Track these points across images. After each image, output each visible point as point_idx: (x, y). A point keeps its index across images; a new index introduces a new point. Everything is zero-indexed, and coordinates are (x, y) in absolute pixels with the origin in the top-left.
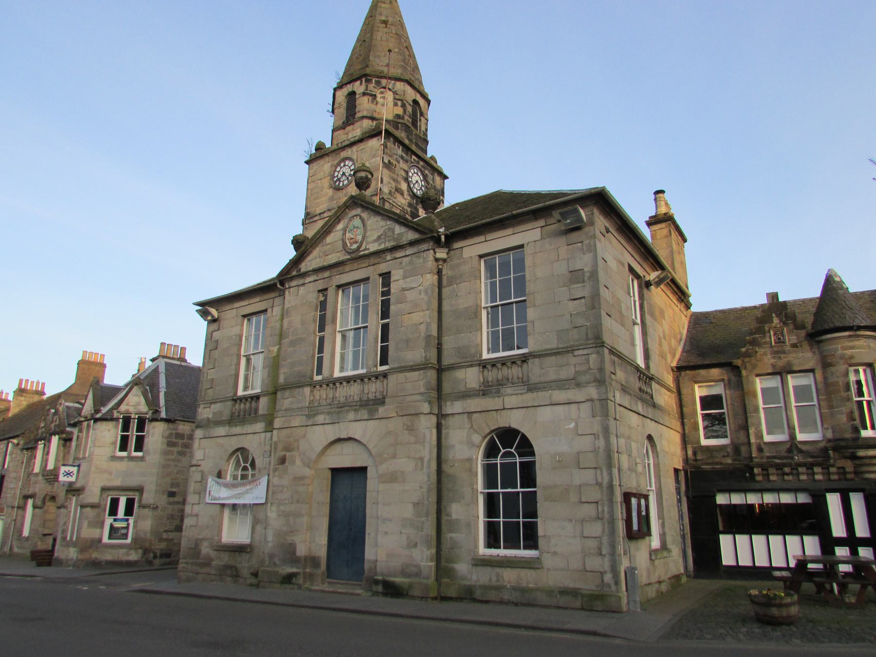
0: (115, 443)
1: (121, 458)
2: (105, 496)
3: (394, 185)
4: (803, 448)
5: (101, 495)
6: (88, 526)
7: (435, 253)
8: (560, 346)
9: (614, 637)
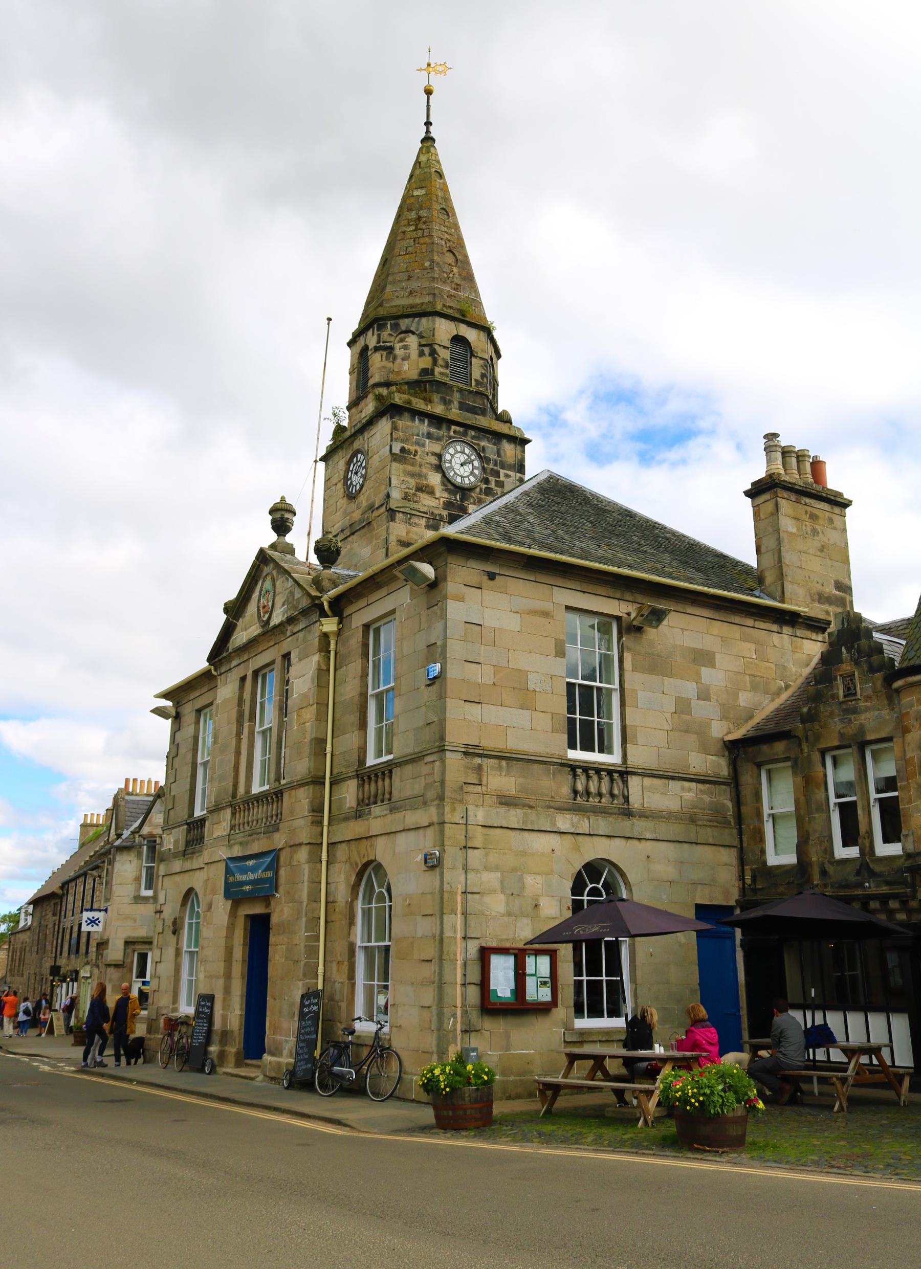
0: (138, 879)
1: (146, 899)
2: (129, 951)
3: (412, 482)
4: (877, 868)
5: (125, 950)
8: (416, 750)
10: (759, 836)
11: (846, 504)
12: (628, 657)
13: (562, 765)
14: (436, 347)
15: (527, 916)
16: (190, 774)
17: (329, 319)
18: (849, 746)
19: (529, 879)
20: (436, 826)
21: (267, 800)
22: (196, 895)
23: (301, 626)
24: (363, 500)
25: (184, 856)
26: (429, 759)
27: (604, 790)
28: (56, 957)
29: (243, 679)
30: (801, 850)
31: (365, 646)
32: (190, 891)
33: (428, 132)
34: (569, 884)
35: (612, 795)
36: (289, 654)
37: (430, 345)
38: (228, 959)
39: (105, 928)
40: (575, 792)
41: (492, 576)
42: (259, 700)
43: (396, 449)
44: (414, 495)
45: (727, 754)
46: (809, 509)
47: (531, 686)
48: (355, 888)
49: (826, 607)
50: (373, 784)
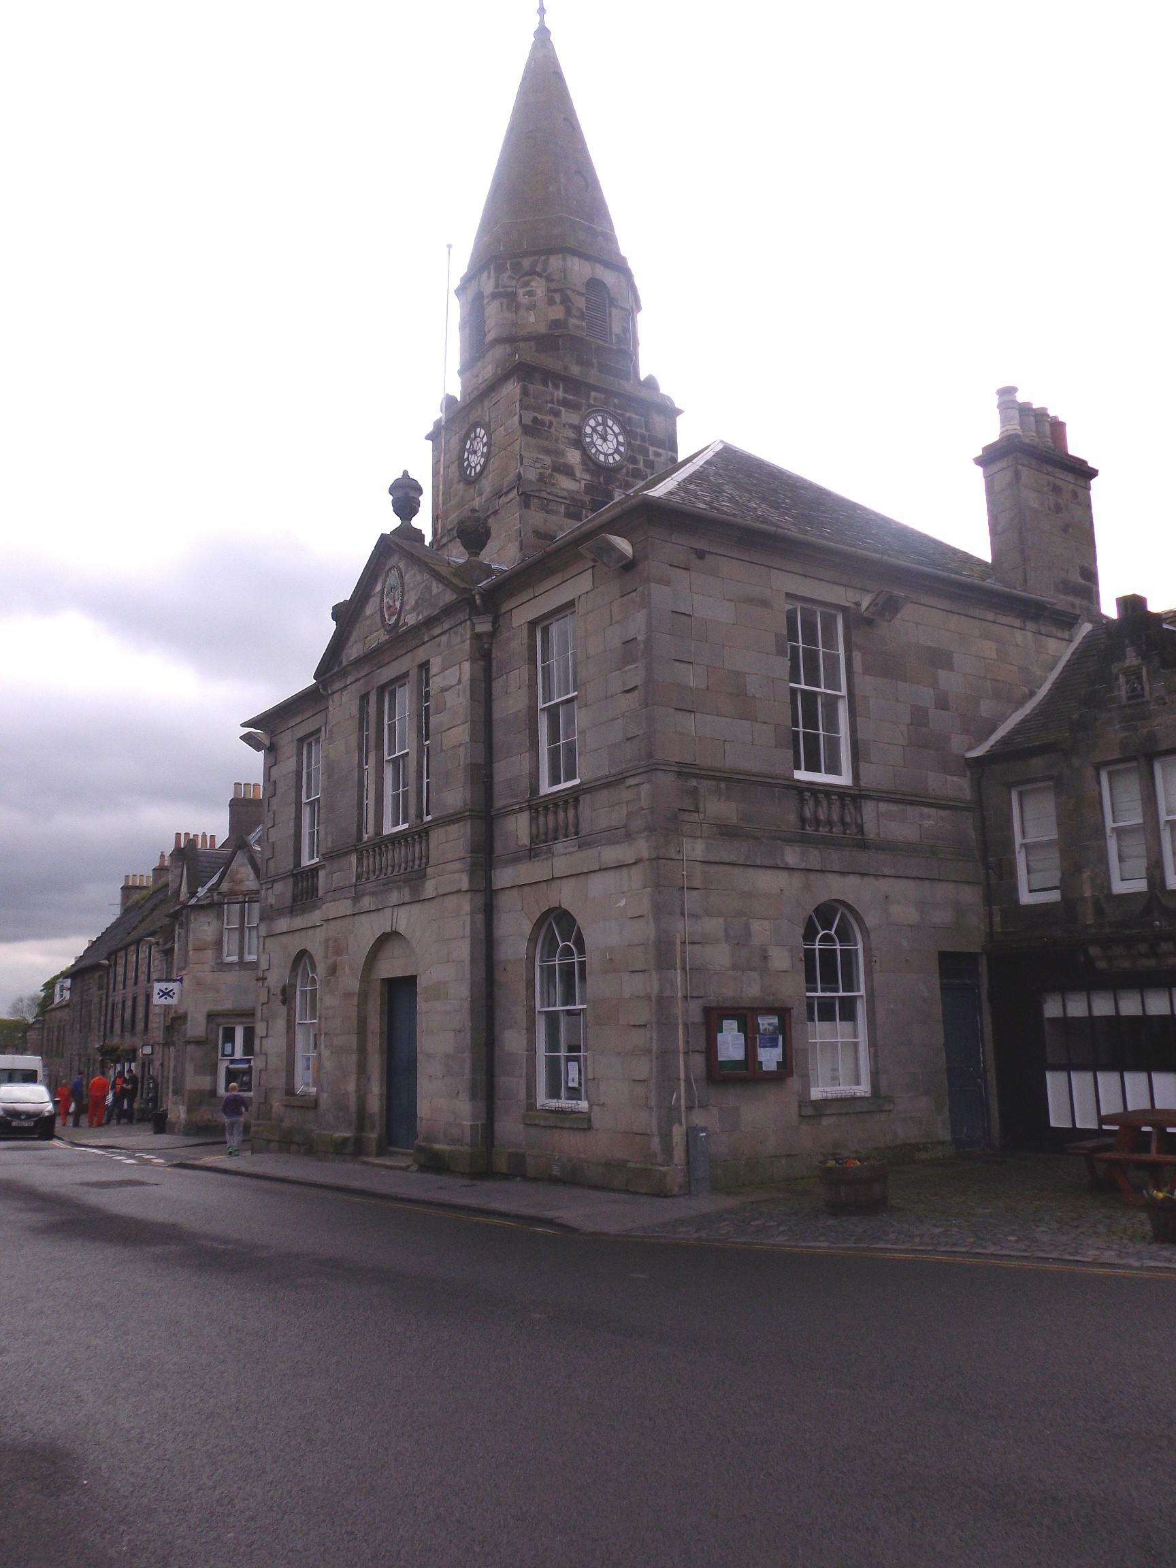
3: (548, 460)
6: (196, 1072)
7: (473, 625)
8: (613, 771)
9: (149, 1184)
10: (1010, 871)
11: (1093, 473)
12: (857, 656)
13: (788, 787)
14: (569, 292)
15: (754, 970)
16: (293, 816)
17: (449, 246)
18: (1134, 758)
19: (756, 925)
20: (647, 863)
21: (406, 841)
22: (311, 957)
23: (446, 626)
24: (487, 485)
25: (291, 912)
26: (632, 781)
27: (835, 818)
28: (105, 1036)
29: (364, 698)
30: (1064, 886)
31: (532, 648)
32: (303, 953)
33: (542, 21)
34: (801, 931)
35: (843, 822)
36: (428, 662)
37: (560, 290)
38: (362, 1031)
39: (180, 1000)
40: (803, 820)
41: (701, 555)
42: (386, 722)
43: (528, 420)
44: (551, 475)
45: (968, 773)
46: (1051, 479)
47: (750, 692)
48: (533, 939)
49: (1071, 598)
50: (551, 818)
